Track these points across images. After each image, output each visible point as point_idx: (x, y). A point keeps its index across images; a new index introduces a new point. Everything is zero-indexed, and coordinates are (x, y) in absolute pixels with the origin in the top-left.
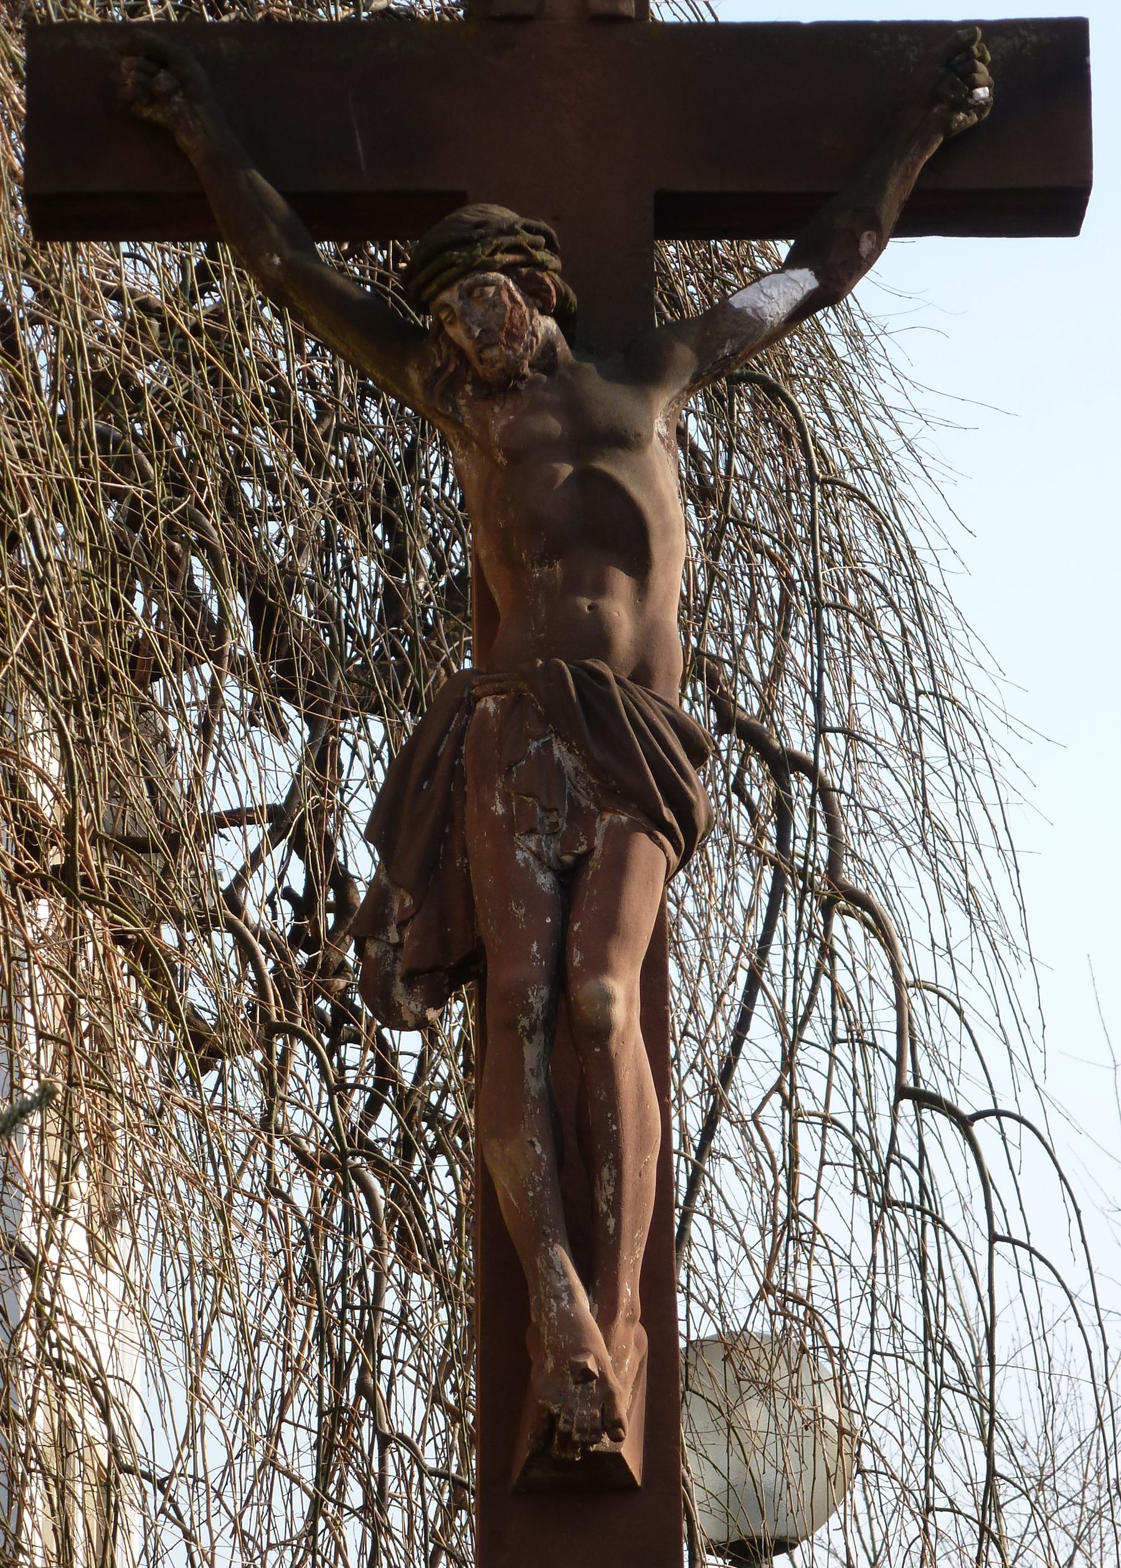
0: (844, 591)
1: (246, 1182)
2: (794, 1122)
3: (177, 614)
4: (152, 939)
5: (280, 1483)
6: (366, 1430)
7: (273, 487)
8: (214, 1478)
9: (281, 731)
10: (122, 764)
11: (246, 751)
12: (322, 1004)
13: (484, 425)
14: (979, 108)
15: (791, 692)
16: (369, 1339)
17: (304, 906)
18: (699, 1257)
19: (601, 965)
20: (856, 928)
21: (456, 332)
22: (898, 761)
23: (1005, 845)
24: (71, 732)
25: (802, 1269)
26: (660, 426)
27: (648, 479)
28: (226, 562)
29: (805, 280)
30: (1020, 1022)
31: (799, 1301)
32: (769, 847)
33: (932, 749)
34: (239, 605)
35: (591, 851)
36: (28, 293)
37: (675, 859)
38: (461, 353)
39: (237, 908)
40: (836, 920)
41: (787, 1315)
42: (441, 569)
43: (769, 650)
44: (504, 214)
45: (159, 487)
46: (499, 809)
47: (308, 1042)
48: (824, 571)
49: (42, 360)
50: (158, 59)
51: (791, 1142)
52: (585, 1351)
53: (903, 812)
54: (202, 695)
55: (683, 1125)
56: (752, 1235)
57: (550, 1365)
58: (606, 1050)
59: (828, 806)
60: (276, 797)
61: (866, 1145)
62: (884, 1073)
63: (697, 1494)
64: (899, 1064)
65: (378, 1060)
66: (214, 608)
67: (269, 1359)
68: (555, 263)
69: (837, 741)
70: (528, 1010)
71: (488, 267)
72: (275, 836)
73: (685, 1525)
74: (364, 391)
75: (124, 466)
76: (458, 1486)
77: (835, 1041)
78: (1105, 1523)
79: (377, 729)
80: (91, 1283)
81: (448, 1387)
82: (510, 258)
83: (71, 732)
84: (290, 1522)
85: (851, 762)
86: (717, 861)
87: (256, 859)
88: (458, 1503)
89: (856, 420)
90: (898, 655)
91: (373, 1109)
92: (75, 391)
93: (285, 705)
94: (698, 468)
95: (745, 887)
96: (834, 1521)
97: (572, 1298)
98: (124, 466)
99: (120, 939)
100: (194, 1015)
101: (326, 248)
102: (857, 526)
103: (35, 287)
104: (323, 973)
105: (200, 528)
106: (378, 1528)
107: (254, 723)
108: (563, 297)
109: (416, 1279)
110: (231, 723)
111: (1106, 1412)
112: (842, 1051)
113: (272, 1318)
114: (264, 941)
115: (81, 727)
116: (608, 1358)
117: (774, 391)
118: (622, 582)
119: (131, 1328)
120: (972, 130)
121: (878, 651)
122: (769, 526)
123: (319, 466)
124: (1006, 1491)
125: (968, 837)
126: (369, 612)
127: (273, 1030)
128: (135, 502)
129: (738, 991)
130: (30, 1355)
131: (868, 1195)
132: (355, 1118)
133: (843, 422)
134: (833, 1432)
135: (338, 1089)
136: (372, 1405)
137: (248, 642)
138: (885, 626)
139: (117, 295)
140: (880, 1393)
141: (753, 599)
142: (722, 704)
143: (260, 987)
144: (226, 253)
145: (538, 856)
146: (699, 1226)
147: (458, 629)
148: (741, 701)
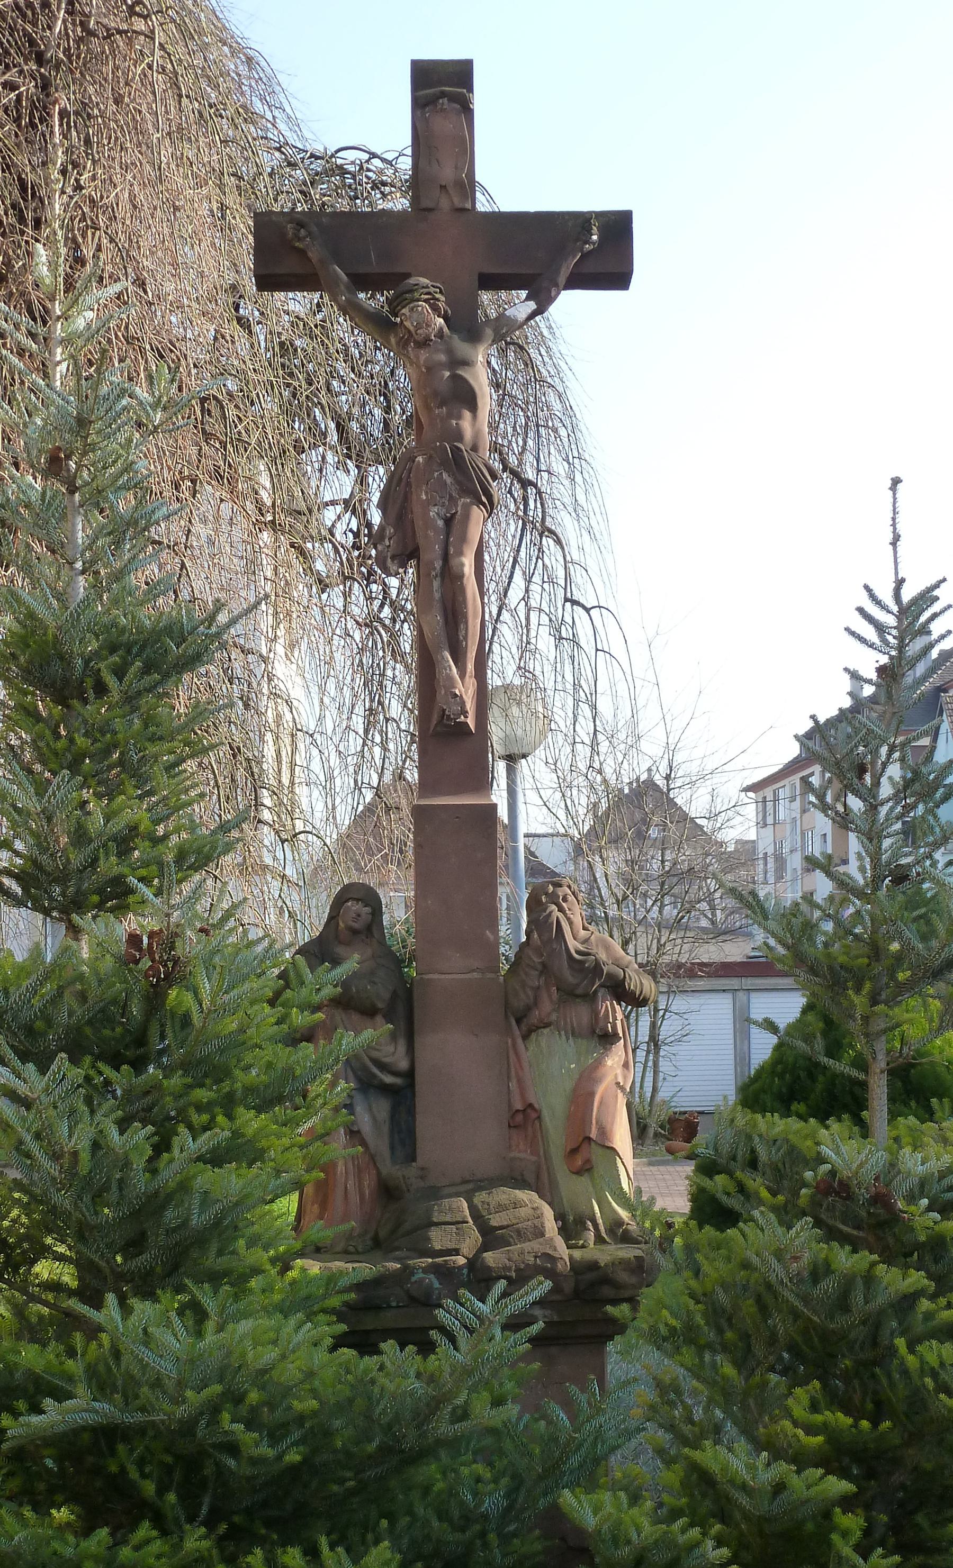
0: (547, 421)
1: (338, 632)
2: (529, 610)
3: (310, 428)
4: (303, 545)
5: (352, 734)
6: (381, 717)
7: (344, 382)
8: (329, 732)
9: (348, 471)
10: (292, 483)
11: (335, 478)
12: (363, 569)
13: (418, 358)
14: (594, 243)
15: (529, 458)
16: (381, 684)
17: (356, 535)
18: (496, 658)
19: (460, 553)
20: (551, 542)
21: (407, 324)
22: (566, 482)
23: (604, 512)
24: (273, 471)
25: (532, 661)
26: (480, 358)
27: (476, 378)
28: (327, 409)
29: (532, 306)
30: (609, 575)
31: (530, 672)
32: (521, 513)
33: (578, 478)
34: (332, 425)
35: (457, 512)
36: (257, 313)
37: (486, 515)
38: (409, 331)
39: (333, 535)
40: (544, 538)
41: (525, 677)
42: (404, 413)
43: (521, 443)
44: (424, 281)
45: (303, 383)
46: (424, 497)
47: (359, 583)
48: (540, 414)
49: (262, 337)
50: (301, 225)
51: (528, 619)
52: (456, 688)
53: (568, 500)
54: (320, 459)
55: (490, 612)
56: (514, 650)
57: (443, 692)
58: (462, 583)
59: (541, 498)
60: (346, 496)
61: (554, 619)
62: (560, 593)
63: (495, 738)
64: (565, 589)
65: (384, 590)
66: (323, 426)
67: (347, 692)
68: (443, 299)
69: (545, 475)
70: (435, 569)
71: (419, 300)
72: (346, 509)
73: (490, 755)
74: (376, 348)
75: (291, 375)
76: (413, 735)
77: (544, 582)
78: (634, 750)
79: (381, 470)
80: (234, 756)
81: (409, 702)
82: (427, 297)
83: (273, 471)
84: (355, 748)
85: (550, 482)
86: (503, 519)
87: (339, 517)
88: (413, 742)
89: (551, 359)
90: (566, 444)
91: (382, 606)
92: (273, 348)
93: (348, 461)
94: (495, 376)
95: (512, 527)
96: (542, 747)
97: (450, 670)
98: (291, 375)
99: (292, 545)
100: (318, 572)
101: (362, 296)
102: (552, 398)
103: (259, 310)
104: (364, 557)
105: (318, 397)
106: (385, 749)
107: (338, 468)
108: (446, 312)
109: (398, 666)
110: (330, 469)
111: (635, 712)
112: (546, 586)
113: (349, 678)
114: (342, 547)
115: (277, 469)
116: (463, 690)
117: (521, 348)
118: (467, 414)
119: (299, 680)
120: (590, 252)
121: (559, 443)
122: (521, 397)
123: (360, 375)
124: (600, 737)
125: (590, 509)
126: (378, 429)
127: (346, 578)
128: (295, 388)
129: (509, 565)
130: (265, 691)
131: (555, 636)
132: (376, 609)
133: (546, 359)
134: (542, 716)
135: (370, 599)
136: (383, 708)
137: (336, 438)
138: (561, 434)
139: (287, 313)
140: (558, 704)
141: (515, 423)
142: (503, 461)
143: (342, 563)
144: (326, 299)
145: (438, 514)
146: (496, 648)
147: (410, 434)
148: (511, 460)
